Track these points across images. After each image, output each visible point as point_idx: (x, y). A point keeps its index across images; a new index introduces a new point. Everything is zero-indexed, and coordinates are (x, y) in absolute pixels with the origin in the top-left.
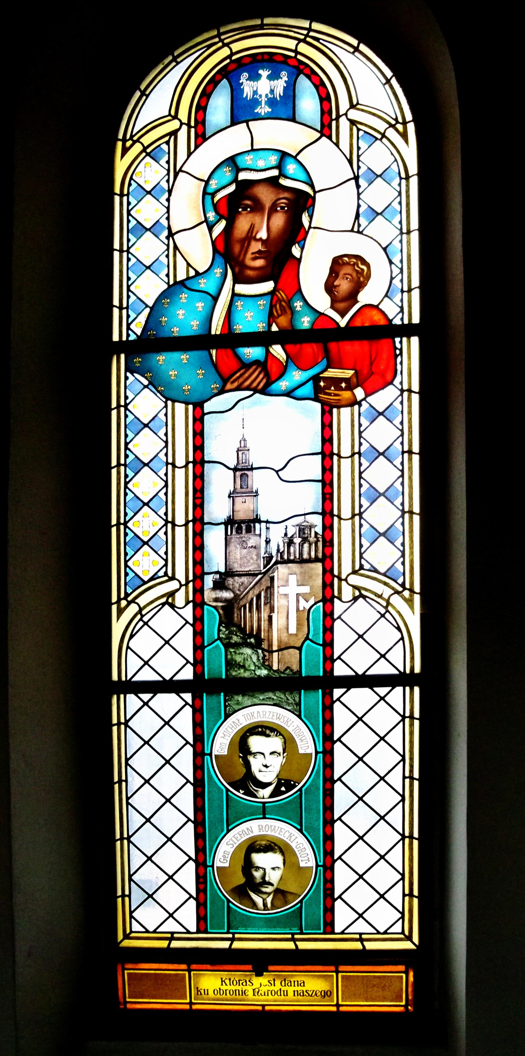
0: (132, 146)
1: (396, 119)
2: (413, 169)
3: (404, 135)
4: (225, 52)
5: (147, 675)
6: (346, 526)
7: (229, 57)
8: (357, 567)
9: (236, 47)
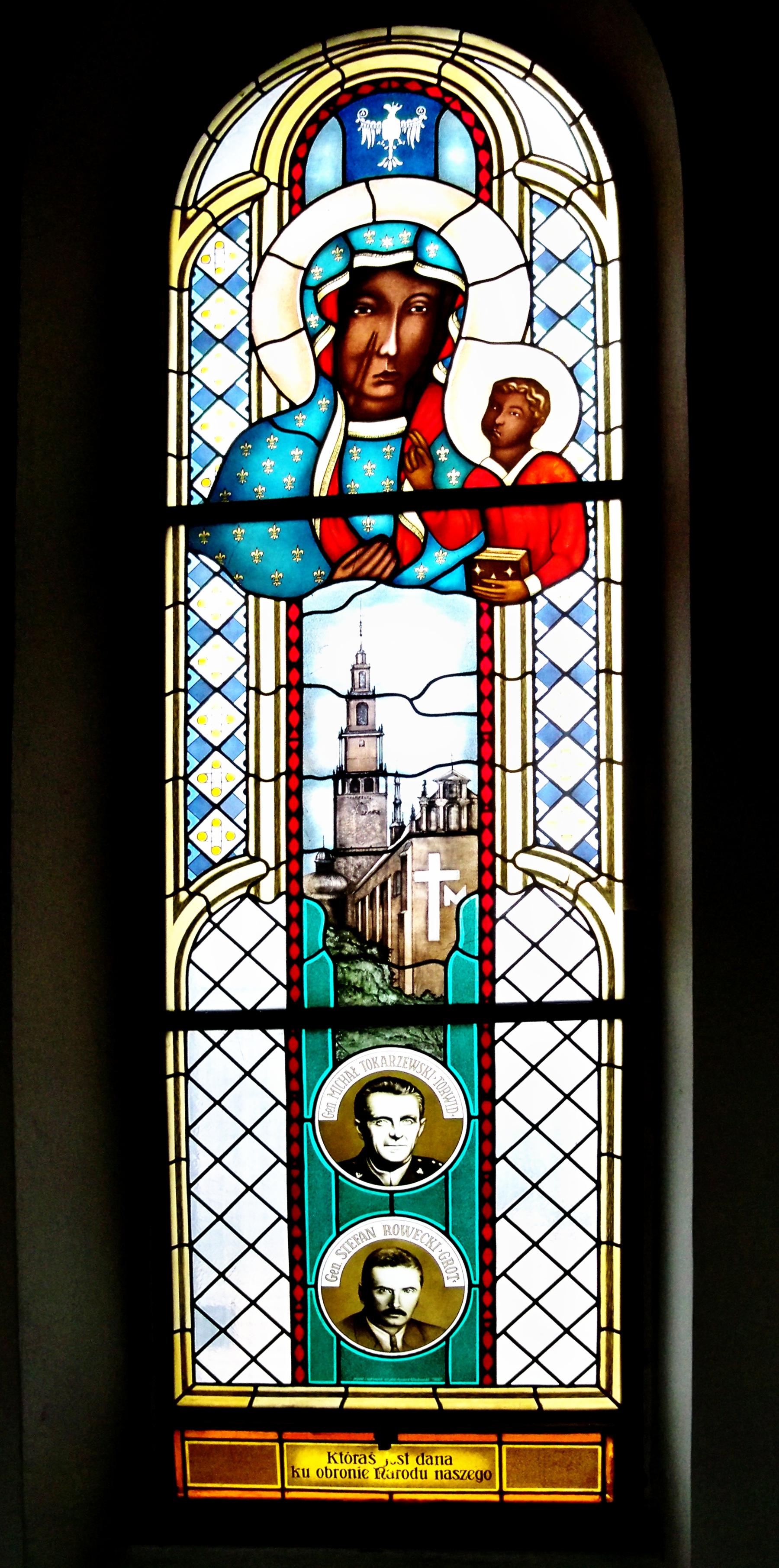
0: (195, 216)
1: (588, 177)
2: (613, 250)
3: (600, 201)
4: (334, 77)
5: (218, 1003)
6: (514, 781)
7: (340, 84)
8: (530, 843)
9: (350, 69)
